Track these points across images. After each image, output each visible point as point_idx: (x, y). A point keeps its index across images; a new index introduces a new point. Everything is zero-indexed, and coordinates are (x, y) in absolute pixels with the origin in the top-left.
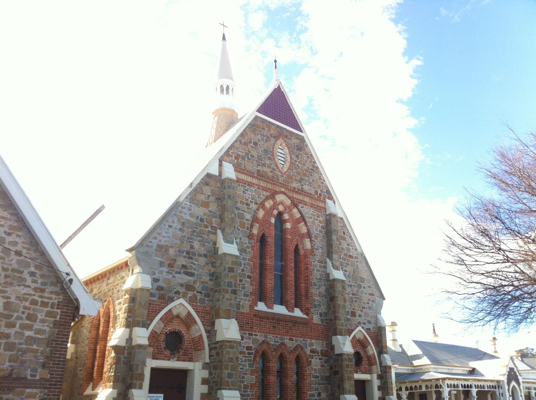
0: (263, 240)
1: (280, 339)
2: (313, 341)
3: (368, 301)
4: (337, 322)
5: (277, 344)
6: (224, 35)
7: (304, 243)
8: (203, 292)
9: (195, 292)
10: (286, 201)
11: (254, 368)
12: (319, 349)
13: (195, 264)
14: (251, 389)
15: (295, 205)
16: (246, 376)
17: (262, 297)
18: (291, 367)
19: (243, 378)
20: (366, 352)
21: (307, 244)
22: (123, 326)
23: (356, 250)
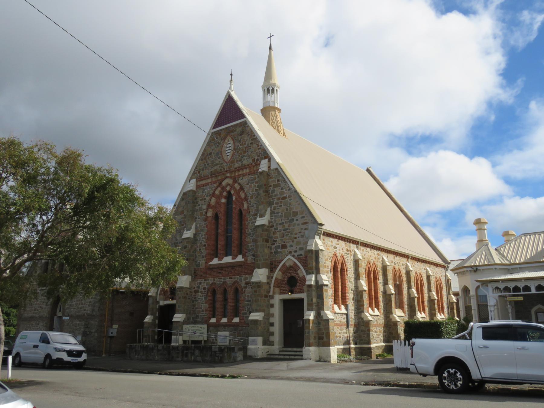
0: (216, 217)
2: (247, 276)
3: (300, 231)
6: (270, 44)
15: (235, 181)
17: (216, 254)
20: (298, 274)
21: (246, 206)
23: (289, 189)
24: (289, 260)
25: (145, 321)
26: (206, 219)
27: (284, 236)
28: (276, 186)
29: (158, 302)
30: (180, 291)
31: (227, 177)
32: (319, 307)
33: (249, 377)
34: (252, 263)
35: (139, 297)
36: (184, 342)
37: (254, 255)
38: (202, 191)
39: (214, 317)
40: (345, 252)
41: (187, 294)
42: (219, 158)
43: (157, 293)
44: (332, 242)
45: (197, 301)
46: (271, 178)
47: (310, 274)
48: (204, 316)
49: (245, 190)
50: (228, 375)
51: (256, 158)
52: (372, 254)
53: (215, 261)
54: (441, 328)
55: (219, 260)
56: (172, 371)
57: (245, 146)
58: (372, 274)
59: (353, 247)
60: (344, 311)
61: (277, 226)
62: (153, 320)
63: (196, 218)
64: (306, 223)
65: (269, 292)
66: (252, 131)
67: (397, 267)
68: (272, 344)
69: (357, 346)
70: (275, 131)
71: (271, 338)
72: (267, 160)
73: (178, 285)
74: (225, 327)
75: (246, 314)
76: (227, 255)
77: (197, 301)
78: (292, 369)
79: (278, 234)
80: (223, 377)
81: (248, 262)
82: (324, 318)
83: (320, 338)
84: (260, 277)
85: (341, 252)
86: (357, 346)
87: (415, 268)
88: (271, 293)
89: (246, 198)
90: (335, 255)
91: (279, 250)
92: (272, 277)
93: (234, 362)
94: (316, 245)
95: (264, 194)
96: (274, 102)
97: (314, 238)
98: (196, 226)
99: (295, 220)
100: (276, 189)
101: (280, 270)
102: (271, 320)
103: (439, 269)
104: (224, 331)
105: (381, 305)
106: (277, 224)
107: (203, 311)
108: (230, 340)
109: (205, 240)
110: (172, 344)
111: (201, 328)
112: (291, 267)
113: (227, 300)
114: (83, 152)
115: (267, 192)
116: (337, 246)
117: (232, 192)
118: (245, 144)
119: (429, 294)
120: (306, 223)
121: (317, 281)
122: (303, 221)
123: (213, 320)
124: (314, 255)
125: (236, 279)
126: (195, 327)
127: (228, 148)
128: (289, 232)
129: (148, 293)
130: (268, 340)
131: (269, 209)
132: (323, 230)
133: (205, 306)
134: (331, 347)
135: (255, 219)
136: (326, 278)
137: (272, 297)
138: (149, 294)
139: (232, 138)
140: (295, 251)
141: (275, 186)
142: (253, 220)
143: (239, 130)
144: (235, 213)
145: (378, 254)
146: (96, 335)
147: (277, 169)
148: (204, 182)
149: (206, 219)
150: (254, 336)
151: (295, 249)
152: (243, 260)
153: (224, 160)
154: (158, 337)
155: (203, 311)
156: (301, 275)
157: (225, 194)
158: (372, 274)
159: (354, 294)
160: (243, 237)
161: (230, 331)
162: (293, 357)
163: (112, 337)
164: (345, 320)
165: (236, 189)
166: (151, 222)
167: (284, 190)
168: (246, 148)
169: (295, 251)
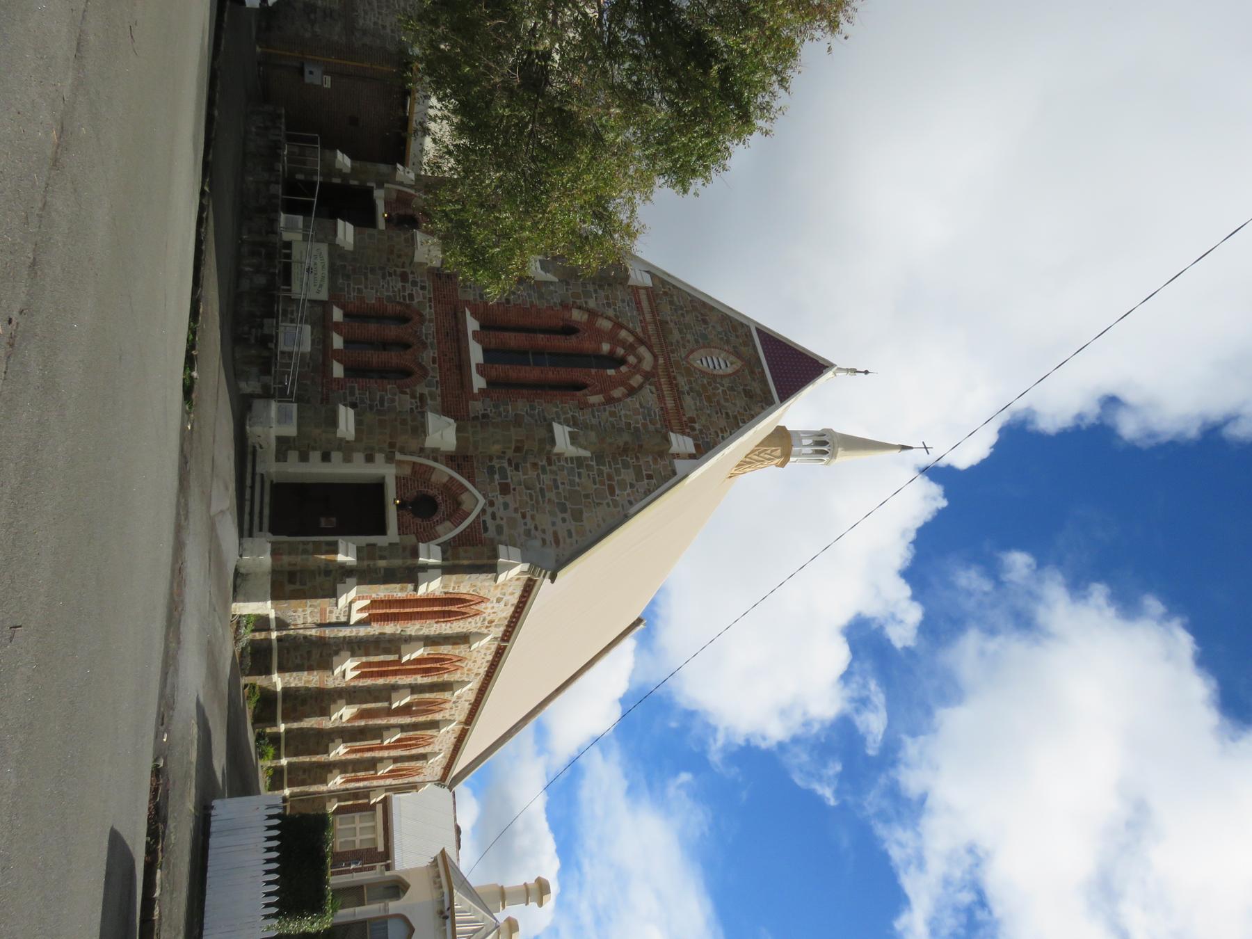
0: (570, 330)
1: (432, 344)
2: (439, 399)
6: (911, 448)
15: (647, 376)
17: (488, 326)
18: (394, 358)
21: (595, 399)
22: (631, 790)
23: (631, 503)
24: (475, 501)
25: (339, 155)
26: (566, 306)
27: (528, 488)
28: (638, 470)
29: (380, 185)
30: (406, 240)
31: (655, 357)
32: (364, 575)
33: (186, 438)
34: (468, 412)
35: (395, 143)
36: (288, 245)
37: (485, 416)
38: (627, 298)
39: (345, 315)
40: (488, 618)
41: (399, 256)
42: (697, 341)
43: (401, 184)
44: (512, 594)
45: (384, 278)
46: (655, 460)
47: (444, 552)
48: (349, 293)
49: (629, 400)
50: (195, 374)
51: (697, 426)
52: (479, 663)
53: (472, 325)
54: (311, 914)
55: (474, 332)
56: (211, 223)
57: (722, 402)
58: (438, 665)
59: (498, 632)
60: (355, 617)
61: (552, 472)
62: (340, 173)
63: (568, 284)
64: (557, 542)
65: (402, 451)
66: (753, 417)
67: (447, 706)
68: (281, 456)
69: (275, 644)
70: (742, 457)
71: (293, 455)
72: (694, 451)
73: (420, 236)
74: (322, 342)
75: (352, 393)
76: (486, 351)
77: (384, 278)
78: (212, 528)
79: (532, 474)
80: (190, 361)
81: (471, 402)
82: (339, 586)
83: (292, 576)
84: (437, 436)
85: (489, 611)
86: (275, 644)
87: (444, 738)
88: (398, 456)
89: (610, 400)
90: (483, 600)
91: (497, 476)
92: (436, 460)
93: (234, 372)
94: (509, 567)
95: (621, 444)
96: (799, 455)
97: (524, 562)
98: (551, 283)
99: (564, 515)
100: (631, 470)
101: (451, 478)
102: (336, 456)
103: (438, 771)
104: (313, 341)
105: (368, 682)
106: (554, 473)
108: (290, 354)
109: (520, 301)
110: (283, 216)
111: (321, 286)
112: (458, 504)
113: (384, 353)
114: (841, 37)
115: (625, 450)
116: (502, 604)
117: (624, 369)
118: (726, 400)
119: (389, 758)
120: (557, 542)
121: (425, 568)
122: (562, 534)
123: (337, 315)
124: (485, 561)
125: (431, 374)
126: (322, 270)
127: (718, 363)
128: (537, 502)
129: (403, 164)
130: (290, 448)
131: (587, 454)
132: (540, 579)
133: (371, 297)
134: (269, 603)
135: (566, 422)
136: (432, 587)
137: (390, 459)
138: (399, 166)
139: (738, 371)
140: (494, 517)
141: (635, 471)
142: (563, 417)
143: (756, 387)
144: (578, 374)
145: (477, 674)
146: (308, 35)
147: (674, 473)
148: (645, 304)
149: (566, 306)
150: (300, 417)
151: (498, 515)
152: (476, 391)
153: (692, 351)
154: (301, 181)
156: (440, 528)
157: (620, 351)
158: (438, 665)
159: (393, 634)
160: (525, 392)
161: (311, 353)
162: (247, 509)
163: (301, 71)
164: (334, 620)
165: (629, 378)
166: (601, 214)
167: (629, 490)
168: (718, 402)
169: (494, 517)
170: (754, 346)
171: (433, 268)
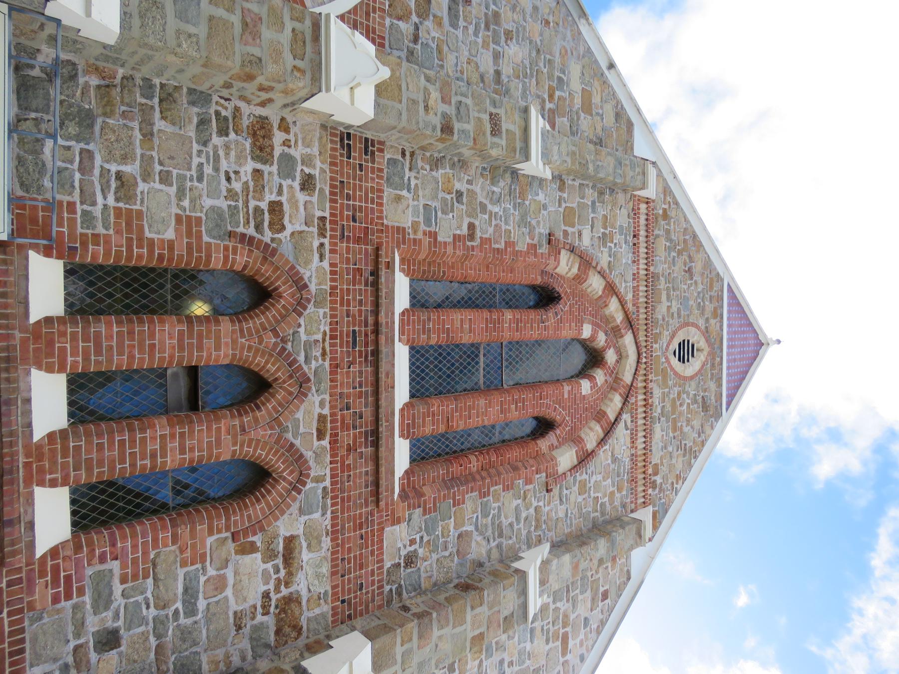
2: (327, 542)
4: (413, 626)
5: (301, 358)
7: (563, 447)
8: (419, 47)
9: (414, 18)
10: (628, 367)
11: (206, 238)
12: (301, 585)
13: (476, 34)
14: (118, 212)
16: (173, 190)
18: (218, 440)
19: (165, 178)
48: (87, 197)
107: (124, 184)
155: (124, 184)
170: (722, 369)
171: (603, 536)
